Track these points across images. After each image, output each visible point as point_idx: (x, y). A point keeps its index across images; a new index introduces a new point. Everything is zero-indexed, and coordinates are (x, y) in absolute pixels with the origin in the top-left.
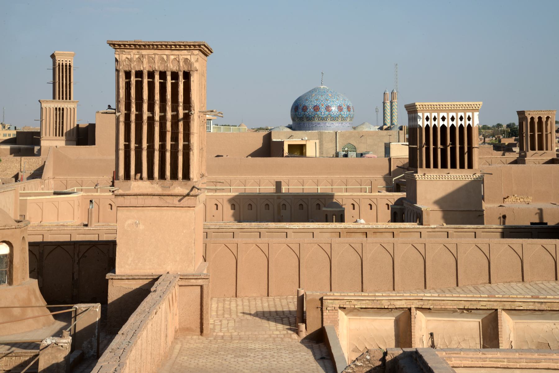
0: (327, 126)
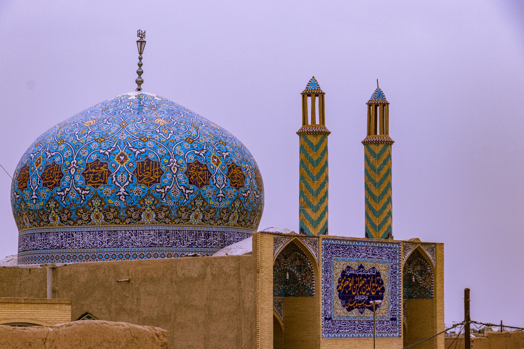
0: (52, 247)
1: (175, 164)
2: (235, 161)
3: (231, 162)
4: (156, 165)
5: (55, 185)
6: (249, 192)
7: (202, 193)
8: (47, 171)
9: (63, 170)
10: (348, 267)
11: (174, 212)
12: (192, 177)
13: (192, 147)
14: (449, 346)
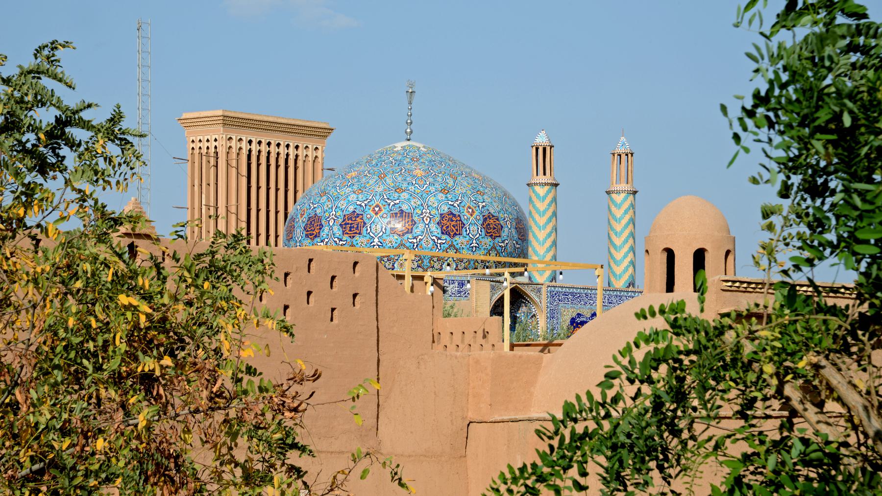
1: (427, 215)
2: (492, 211)
3: (487, 213)
4: (409, 216)
5: (316, 236)
6: (506, 242)
7: (455, 243)
8: (309, 223)
9: (323, 222)
10: (578, 314)
11: (426, 262)
12: (444, 228)
13: (446, 197)
14: (376, 338)
